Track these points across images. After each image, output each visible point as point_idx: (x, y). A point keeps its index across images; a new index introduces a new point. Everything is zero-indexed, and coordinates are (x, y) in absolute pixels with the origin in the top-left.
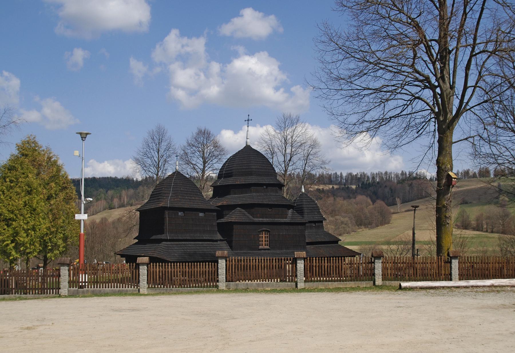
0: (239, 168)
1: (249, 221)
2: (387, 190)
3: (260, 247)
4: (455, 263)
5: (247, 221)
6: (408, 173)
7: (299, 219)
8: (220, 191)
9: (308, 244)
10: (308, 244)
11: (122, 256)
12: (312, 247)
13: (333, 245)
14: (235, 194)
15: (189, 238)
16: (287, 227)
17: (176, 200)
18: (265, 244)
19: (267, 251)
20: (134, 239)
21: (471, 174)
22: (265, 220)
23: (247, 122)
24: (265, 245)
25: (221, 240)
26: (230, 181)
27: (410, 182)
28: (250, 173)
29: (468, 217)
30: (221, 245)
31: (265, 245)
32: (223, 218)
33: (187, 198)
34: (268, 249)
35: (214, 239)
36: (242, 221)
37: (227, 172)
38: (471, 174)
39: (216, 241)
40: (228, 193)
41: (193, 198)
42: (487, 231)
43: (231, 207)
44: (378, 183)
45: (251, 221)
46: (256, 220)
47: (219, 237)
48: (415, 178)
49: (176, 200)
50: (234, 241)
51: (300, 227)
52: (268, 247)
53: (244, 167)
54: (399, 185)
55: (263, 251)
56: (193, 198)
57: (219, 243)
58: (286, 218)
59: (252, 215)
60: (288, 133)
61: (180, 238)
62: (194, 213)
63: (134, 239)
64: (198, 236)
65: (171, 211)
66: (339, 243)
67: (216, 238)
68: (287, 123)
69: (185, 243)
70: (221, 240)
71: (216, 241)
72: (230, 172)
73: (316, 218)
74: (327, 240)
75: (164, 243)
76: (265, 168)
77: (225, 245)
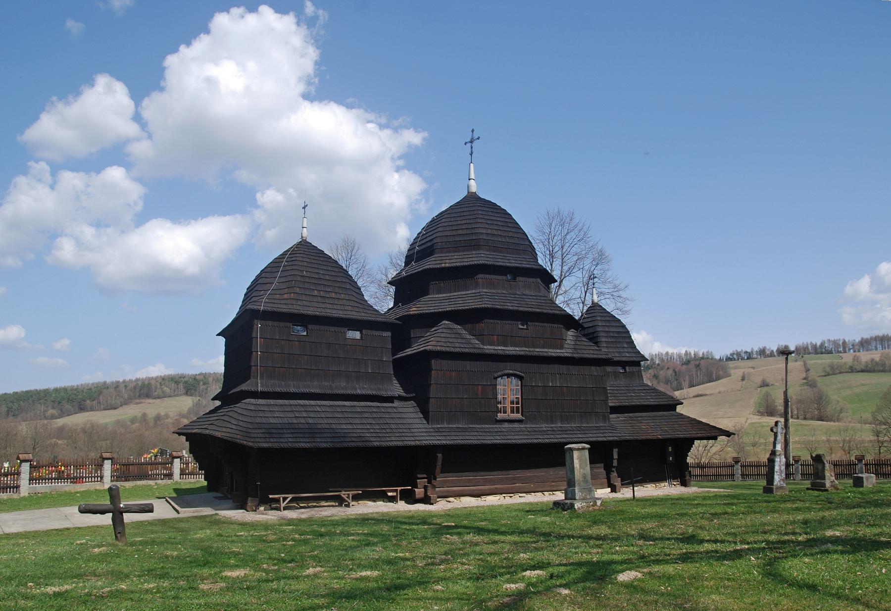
0: (449, 233)
1: (471, 351)
2: (670, 372)
3: (500, 416)
4: (107, 465)
5: (467, 350)
6: (693, 354)
7: (589, 351)
8: (406, 287)
9: (615, 410)
10: (615, 410)
11: (180, 434)
12: (622, 417)
13: (665, 413)
14: (439, 292)
15: (318, 391)
16: (564, 369)
17: (286, 296)
18: (512, 409)
19: (516, 425)
20: (214, 399)
21: (768, 352)
22: (511, 350)
23: (469, 145)
24: (512, 412)
25: (400, 398)
26: (430, 263)
27: (697, 363)
28: (474, 245)
29: (774, 401)
30: (401, 410)
31: (512, 412)
32: (410, 347)
33: (316, 293)
34: (520, 421)
35: (383, 393)
36: (452, 350)
37: (423, 247)
38: (768, 352)
39: (390, 399)
40: (424, 292)
41: (333, 295)
42: (798, 418)
43: (431, 320)
44: (659, 365)
45: (476, 351)
46: (489, 349)
47: (396, 389)
48: (702, 358)
49: (286, 296)
50: (432, 401)
51: (595, 370)
52: (519, 416)
53: (461, 232)
54: (685, 366)
55: (506, 425)
56: (333, 295)
57: (396, 404)
58: (561, 347)
59: (479, 336)
60: (555, 241)
61: (293, 390)
62: (332, 329)
63: (214, 399)
64: (341, 386)
65: (271, 323)
66: (679, 409)
67: (390, 394)
68: (553, 225)
69: (307, 402)
70: (400, 398)
71: (390, 399)
72: (429, 244)
73: (627, 356)
74: (652, 401)
75: (247, 401)
76: (510, 234)
77: (412, 410)
